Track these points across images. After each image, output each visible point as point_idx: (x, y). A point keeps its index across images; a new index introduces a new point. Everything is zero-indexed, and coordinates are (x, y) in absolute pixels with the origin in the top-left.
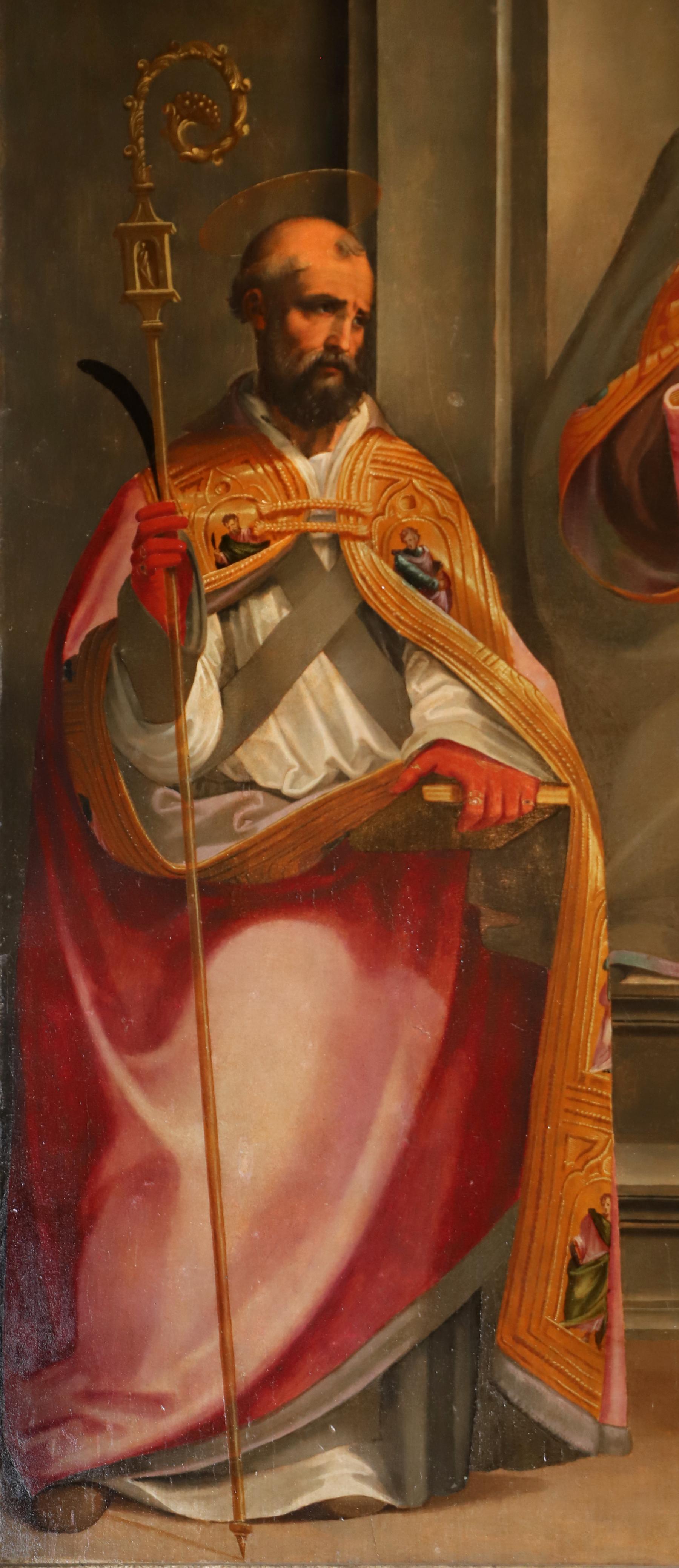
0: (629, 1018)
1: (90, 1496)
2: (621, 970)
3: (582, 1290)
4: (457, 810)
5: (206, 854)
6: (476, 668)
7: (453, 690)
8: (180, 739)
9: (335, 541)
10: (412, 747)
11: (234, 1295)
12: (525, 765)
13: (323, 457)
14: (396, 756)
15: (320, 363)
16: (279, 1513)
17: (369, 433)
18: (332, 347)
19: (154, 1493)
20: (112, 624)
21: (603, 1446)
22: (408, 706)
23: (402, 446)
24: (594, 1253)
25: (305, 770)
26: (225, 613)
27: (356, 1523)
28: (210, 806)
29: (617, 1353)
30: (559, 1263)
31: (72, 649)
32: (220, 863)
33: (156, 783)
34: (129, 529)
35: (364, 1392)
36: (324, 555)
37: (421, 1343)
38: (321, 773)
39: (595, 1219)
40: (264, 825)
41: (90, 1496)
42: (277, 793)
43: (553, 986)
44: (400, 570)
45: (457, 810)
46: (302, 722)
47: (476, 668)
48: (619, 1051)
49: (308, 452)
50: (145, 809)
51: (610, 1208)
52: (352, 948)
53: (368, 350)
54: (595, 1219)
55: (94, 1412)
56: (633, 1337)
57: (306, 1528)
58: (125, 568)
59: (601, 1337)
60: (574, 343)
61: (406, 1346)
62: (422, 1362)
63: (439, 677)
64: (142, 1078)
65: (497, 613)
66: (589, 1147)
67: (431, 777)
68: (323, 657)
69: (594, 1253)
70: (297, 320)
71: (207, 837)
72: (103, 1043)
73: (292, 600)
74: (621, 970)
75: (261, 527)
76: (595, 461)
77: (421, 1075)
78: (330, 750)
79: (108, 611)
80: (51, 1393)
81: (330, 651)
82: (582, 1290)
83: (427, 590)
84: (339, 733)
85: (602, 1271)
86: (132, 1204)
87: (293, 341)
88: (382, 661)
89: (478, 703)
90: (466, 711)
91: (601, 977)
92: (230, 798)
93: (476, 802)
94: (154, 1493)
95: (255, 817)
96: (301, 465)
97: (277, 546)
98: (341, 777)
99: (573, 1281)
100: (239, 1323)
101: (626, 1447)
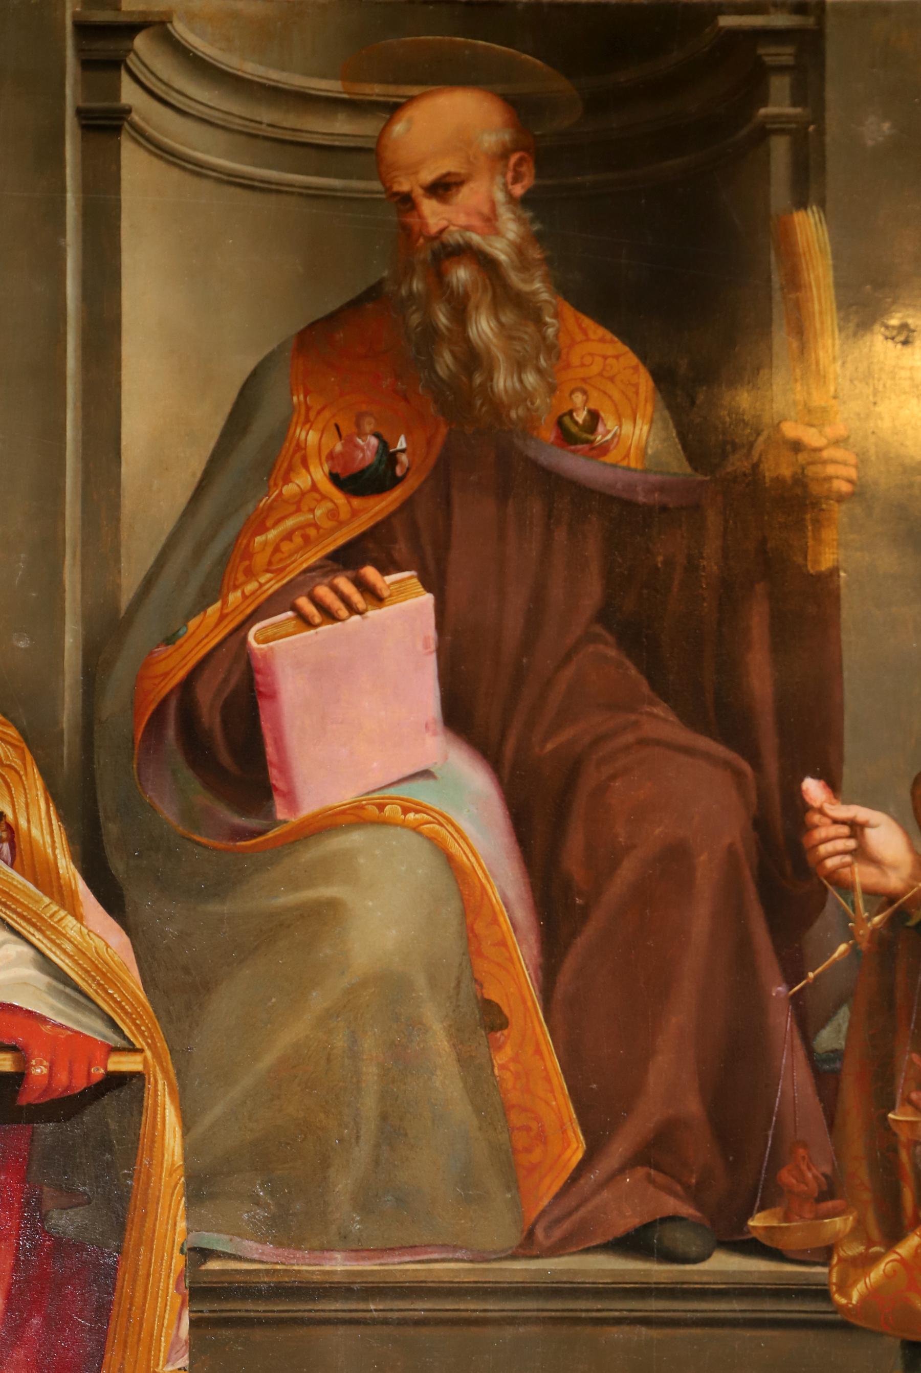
0: (207, 1308)
60: (149, 582)
65: (67, 868)
74: (202, 1254)
76: (173, 704)
89: (46, 964)
90: (31, 972)
91: (178, 1262)
93: (39, 1070)
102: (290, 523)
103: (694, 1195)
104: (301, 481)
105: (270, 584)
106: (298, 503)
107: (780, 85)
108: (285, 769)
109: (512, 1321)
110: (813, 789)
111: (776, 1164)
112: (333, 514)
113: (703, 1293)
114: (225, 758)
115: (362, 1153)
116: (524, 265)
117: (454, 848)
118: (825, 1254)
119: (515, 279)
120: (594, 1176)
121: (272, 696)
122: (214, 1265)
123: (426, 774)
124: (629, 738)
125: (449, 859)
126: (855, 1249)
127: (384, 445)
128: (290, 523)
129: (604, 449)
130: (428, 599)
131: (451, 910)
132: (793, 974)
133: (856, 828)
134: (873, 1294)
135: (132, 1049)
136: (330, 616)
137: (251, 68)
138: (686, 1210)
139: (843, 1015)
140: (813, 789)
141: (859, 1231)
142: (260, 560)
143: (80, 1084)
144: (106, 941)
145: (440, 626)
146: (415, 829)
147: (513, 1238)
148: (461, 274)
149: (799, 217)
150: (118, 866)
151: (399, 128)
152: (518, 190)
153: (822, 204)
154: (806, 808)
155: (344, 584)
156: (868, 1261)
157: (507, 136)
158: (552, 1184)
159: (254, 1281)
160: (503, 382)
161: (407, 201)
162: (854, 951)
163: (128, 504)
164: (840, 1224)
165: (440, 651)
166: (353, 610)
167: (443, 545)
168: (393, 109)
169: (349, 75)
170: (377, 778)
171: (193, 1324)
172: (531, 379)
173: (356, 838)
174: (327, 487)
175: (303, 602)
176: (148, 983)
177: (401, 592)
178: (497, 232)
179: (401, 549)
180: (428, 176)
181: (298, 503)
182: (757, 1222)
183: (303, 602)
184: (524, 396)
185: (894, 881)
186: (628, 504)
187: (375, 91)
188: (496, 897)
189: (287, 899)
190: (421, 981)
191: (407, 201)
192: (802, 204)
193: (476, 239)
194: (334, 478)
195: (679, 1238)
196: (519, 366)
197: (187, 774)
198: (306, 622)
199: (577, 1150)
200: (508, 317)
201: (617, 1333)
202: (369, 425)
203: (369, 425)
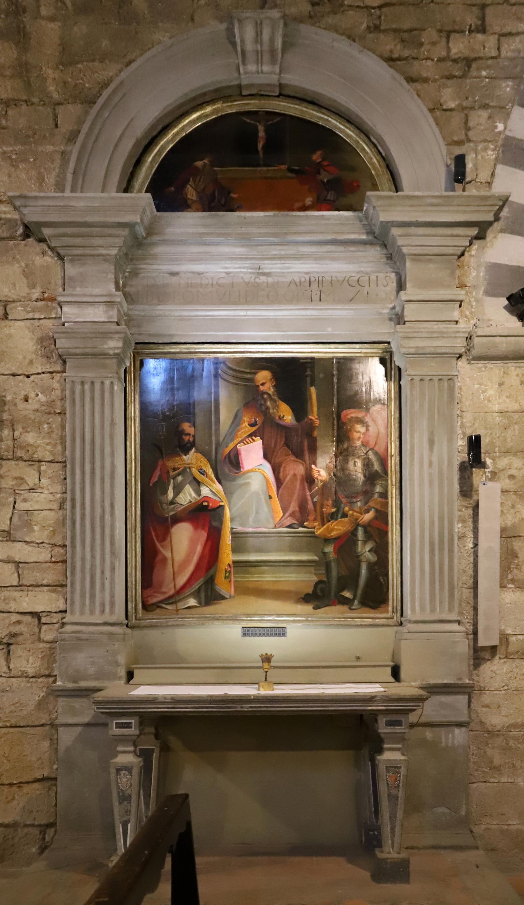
0: (233, 535)
1: (155, 607)
2: (232, 528)
3: (227, 575)
4: (208, 506)
5: (171, 513)
6: (210, 485)
7: (207, 489)
8: (167, 497)
9: (190, 468)
10: (201, 497)
11: (176, 577)
12: (217, 499)
13: (188, 456)
14: (199, 498)
15: (187, 443)
16: (183, 608)
17: (195, 452)
18: (189, 440)
19: (164, 606)
20: (157, 481)
21: (230, 597)
22: (200, 491)
23: (199, 454)
24: (229, 569)
25: (185, 501)
26: (174, 479)
27: (194, 609)
28: (172, 506)
29: (232, 584)
30: (224, 572)
31: (151, 485)
32: (173, 515)
33: (164, 503)
34: (159, 468)
35: (195, 590)
36: (188, 470)
37: (203, 584)
38: (188, 501)
39: (229, 565)
40: (179, 509)
41: (155, 607)
42: (181, 504)
43: (222, 531)
44: (199, 472)
45: (208, 506)
46: (185, 494)
47: (210, 485)
48: (232, 540)
49: (185, 456)
50: (162, 507)
51: (231, 563)
52: (193, 526)
53: (194, 440)
54: (229, 565)
55: (155, 594)
56: (235, 581)
57: (187, 610)
58: (158, 473)
59: (230, 581)
60: (224, 439)
61: (201, 583)
62: (203, 586)
63: (205, 487)
64: (162, 546)
65: (214, 478)
66: (228, 554)
67: (204, 501)
68: (188, 485)
69: (229, 569)
70: (184, 437)
71: (171, 511)
72: (156, 541)
73: (183, 476)
74: (232, 528)
75: (179, 466)
76: (227, 457)
77: (203, 544)
78: (189, 498)
79: (156, 479)
80: (18, 184)
81: (189, 484)
82: (227, 575)
83: (203, 475)
84: (190, 495)
85: (230, 572)
86: (168, 413)
87: (183, 439)
88: (197, 485)
89: (211, 490)
90: (209, 492)
91: (229, 529)
92: (175, 505)
93: (211, 505)
94: (164, 606)
95: (178, 508)
96: (184, 457)
97: (181, 469)
98: (191, 502)
99: (226, 574)
100: (177, 581)
101: (234, 597)
102: (243, 431)
103: (297, 520)
104: (244, 425)
105: (240, 439)
106: (244, 428)
107: (309, 370)
108: (242, 464)
109: (273, 537)
110: (313, 466)
111: (308, 516)
112: (249, 429)
113: (298, 533)
114: (234, 463)
115: (254, 515)
116: (274, 395)
117: (265, 475)
118: (314, 528)
119: (273, 397)
120: (283, 518)
121: (240, 454)
122: (234, 530)
123: (261, 465)
124: (289, 459)
125: (264, 476)
126: (318, 527)
127: (255, 420)
128: (243, 431)
129: (285, 420)
130: (261, 441)
131: (265, 483)
132: (310, 491)
133: (319, 471)
134: (321, 532)
135: (223, 502)
136: (248, 443)
137: (237, 368)
138: (296, 522)
139: (317, 497)
140: (313, 466)
141: (319, 525)
142: (239, 436)
143: (216, 506)
144: (499, 334)
145: (263, 445)
146: (260, 472)
147: (273, 526)
148: (265, 396)
149: (311, 388)
150: (220, 477)
151: (257, 376)
152: (273, 384)
153: (314, 386)
154: (312, 469)
155: (250, 439)
156: (320, 529)
157: (271, 377)
158: (278, 519)
159: (471, 545)
160: (271, 411)
161: (258, 386)
162: (318, 488)
163: (221, 428)
164: (316, 524)
165: (263, 448)
166: (251, 442)
167: (263, 434)
168: (255, 373)
169: (251, 369)
170: (254, 465)
171: (232, 537)
172: (275, 410)
173: (252, 473)
174: (247, 425)
175: (245, 442)
176: (225, 493)
177: (258, 440)
178: (270, 390)
179: (258, 434)
180: (261, 382)
181: (244, 428)
182: (305, 524)
183: (245, 442)
184: (274, 413)
185: (324, 479)
186: (288, 428)
187: (253, 371)
188: (271, 481)
189: (243, 482)
190: (261, 492)
191: (258, 386)
192: (312, 386)
193: (267, 391)
194: (249, 424)
195: (295, 526)
196: (273, 409)
197: (229, 465)
198: (245, 444)
199: (282, 514)
200: (272, 402)
201: (287, 538)
202: (253, 417)
203: (253, 417)
